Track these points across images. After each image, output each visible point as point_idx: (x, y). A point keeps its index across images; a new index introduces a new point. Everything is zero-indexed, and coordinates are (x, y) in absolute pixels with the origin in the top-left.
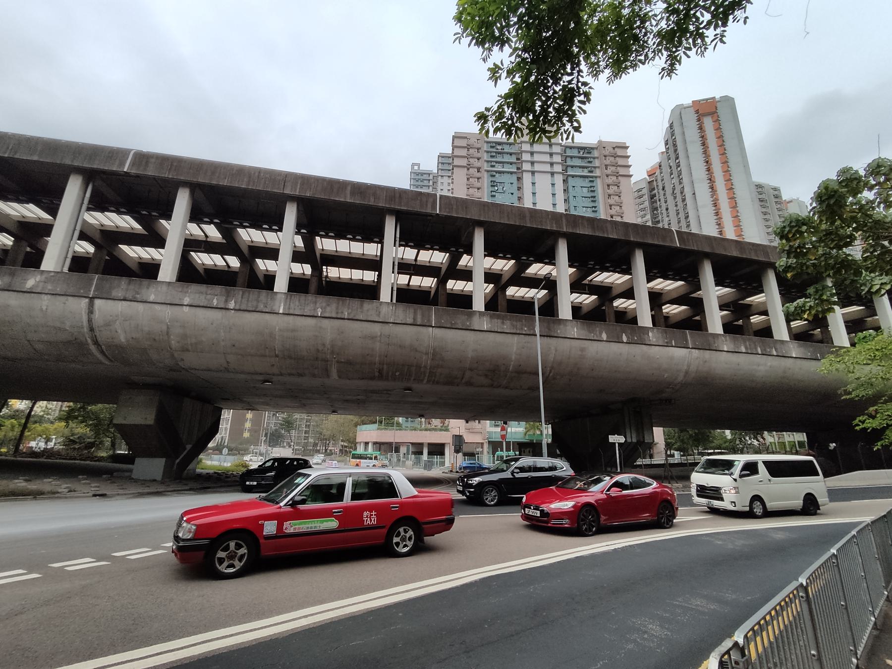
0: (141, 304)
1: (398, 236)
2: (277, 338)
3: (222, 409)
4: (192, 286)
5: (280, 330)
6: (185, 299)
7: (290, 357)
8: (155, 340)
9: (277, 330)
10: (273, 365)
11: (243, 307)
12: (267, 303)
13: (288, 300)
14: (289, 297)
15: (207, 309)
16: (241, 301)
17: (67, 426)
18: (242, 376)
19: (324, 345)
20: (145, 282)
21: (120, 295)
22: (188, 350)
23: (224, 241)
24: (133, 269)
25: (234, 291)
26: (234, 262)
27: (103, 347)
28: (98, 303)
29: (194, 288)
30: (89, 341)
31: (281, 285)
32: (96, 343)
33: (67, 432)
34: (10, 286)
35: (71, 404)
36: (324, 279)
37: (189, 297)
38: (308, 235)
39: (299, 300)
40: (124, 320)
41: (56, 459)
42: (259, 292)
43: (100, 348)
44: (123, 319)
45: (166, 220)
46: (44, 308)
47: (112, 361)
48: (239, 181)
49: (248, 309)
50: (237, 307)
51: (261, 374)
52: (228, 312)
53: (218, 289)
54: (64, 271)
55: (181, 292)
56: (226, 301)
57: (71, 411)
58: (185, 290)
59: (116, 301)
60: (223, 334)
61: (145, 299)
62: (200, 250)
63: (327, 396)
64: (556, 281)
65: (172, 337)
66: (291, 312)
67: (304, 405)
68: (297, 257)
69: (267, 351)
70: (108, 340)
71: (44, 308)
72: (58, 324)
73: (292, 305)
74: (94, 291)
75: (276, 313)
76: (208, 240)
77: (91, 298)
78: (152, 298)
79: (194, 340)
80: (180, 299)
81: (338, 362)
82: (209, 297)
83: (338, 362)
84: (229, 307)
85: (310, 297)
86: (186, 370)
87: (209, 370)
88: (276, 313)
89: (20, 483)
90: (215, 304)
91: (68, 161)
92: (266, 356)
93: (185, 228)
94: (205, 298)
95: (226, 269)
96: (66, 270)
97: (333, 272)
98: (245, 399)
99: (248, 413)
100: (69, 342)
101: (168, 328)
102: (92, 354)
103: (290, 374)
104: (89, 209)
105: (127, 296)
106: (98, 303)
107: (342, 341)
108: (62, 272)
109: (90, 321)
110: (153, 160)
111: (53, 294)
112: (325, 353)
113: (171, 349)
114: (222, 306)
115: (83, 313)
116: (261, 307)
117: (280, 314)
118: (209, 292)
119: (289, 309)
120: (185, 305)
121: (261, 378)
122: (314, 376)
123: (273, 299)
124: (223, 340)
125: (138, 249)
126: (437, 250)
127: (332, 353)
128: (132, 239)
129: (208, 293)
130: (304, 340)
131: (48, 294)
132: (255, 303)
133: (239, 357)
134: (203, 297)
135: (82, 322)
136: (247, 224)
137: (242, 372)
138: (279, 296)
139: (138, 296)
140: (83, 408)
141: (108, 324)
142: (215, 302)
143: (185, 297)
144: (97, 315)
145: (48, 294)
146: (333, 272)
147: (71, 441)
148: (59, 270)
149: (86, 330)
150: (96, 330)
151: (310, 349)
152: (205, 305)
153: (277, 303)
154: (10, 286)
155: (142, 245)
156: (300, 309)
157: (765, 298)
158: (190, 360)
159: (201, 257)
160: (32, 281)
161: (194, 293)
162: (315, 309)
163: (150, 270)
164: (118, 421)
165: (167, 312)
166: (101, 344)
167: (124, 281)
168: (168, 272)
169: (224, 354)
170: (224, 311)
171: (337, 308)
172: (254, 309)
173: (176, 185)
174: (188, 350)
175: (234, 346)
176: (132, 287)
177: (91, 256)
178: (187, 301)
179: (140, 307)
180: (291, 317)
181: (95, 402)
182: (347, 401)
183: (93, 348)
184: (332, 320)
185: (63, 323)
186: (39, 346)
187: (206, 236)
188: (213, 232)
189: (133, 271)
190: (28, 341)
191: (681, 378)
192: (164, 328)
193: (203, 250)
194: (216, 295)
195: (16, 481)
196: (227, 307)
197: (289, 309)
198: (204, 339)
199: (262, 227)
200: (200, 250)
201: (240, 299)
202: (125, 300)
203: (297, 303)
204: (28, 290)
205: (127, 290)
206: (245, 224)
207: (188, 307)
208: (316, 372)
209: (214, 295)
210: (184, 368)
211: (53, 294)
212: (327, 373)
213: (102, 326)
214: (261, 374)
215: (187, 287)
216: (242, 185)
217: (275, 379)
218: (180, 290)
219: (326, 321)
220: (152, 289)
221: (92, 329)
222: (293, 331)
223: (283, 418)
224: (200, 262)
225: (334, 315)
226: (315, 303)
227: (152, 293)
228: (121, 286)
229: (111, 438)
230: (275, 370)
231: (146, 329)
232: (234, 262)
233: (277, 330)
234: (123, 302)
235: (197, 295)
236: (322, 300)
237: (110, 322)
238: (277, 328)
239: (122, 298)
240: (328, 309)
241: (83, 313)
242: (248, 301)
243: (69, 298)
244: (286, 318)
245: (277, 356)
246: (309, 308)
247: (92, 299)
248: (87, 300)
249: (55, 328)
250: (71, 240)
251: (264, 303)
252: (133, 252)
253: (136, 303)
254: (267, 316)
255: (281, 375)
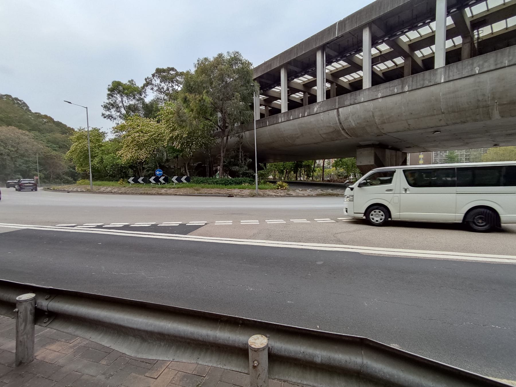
0: (358, 104)
1: (325, 59)
2: (442, 100)
3: (407, 153)
4: (381, 86)
5: (443, 95)
6: (379, 94)
7: (454, 112)
8: (368, 121)
9: (441, 95)
10: (441, 120)
11: (414, 87)
12: (431, 79)
13: (447, 71)
14: (447, 69)
15: (392, 96)
16: (412, 84)
17: (336, 169)
18: (419, 131)
19: (484, 95)
20: (358, 92)
21: (348, 103)
22: (385, 123)
23: (392, 50)
24: (347, 88)
25: (406, 79)
26: (400, 61)
27: (346, 130)
28: (340, 110)
29: (382, 86)
30: (340, 128)
31: (440, 62)
32: (343, 129)
33: (336, 172)
34: (310, 113)
35: (336, 159)
36: (476, 42)
37: (380, 92)
38: (458, 12)
39: (457, 67)
40: (352, 115)
41: (336, 182)
42: (424, 74)
43: (345, 131)
44: (352, 115)
45: (358, 54)
46: (322, 119)
47: (351, 136)
48: (397, 2)
49: (418, 88)
50: (410, 89)
51: (431, 128)
52: (404, 94)
53: (396, 82)
54: (325, 100)
55: (376, 91)
56: (403, 88)
57: (336, 162)
58: (378, 89)
59: (347, 107)
60: (403, 108)
61: (359, 101)
62: (378, 62)
63: (489, 134)
64: (330, 98)
65: (376, 118)
66: (451, 78)
67: (467, 143)
68: (450, 34)
69: (435, 111)
70: (348, 127)
71: (322, 119)
72: (328, 125)
73: (451, 74)
74: (338, 105)
75: (438, 84)
76: (382, 53)
77: (337, 109)
78: (362, 100)
79: (387, 117)
80: (376, 95)
81: (499, 105)
82: (391, 89)
83: (499, 105)
84: (405, 91)
85: (466, 62)
86: (385, 134)
87: (398, 132)
88: (438, 84)
89: (330, 191)
90: (396, 92)
91: (356, 26)
92: (434, 115)
93: (370, 51)
94: (390, 90)
95: (395, 67)
96: (325, 98)
97: (485, 32)
98: (421, 146)
99: (420, 155)
100: (332, 132)
101: (373, 113)
102: (343, 135)
103: (454, 124)
104: (326, 66)
105: (351, 103)
106: (340, 110)
107: (504, 87)
108: (324, 101)
109: (339, 119)
110: (347, 22)
111: (323, 112)
112: (486, 101)
113: (376, 124)
114: (400, 91)
115: (336, 117)
116: (427, 83)
117: (442, 83)
118: (391, 86)
119: (449, 77)
120: (379, 98)
121: (432, 130)
122: (476, 120)
123: (435, 75)
124: (404, 112)
125: (348, 77)
126: (430, 22)
127: (493, 99)
128: (344, 72)
129: (391, 86)
130: (464, 96)
131: (322, 112)
132: (422, 82)
133: (416, 119)
134: (388, 90)
135: (336, 121)
136: (429, 21)
137: (419, 129)
138: (439, 71)
139: (356, 101)
140: (340, 160)
141: (346, 119)
142: (396, 90)
143: (379, 93)
144: (341, 116)
145: (322, 112)
146: (485, 32)
147: (339, 175)
148: (323, 100)
149: (338, 124)
150: (342, 123)
151: (470, 102)
152: (390, 94)
153: (438, 76)
154: (310, 113)
155: (349, 74)
156: (459, 74)
157: (241, 221)
158: (387, 128)
159: (359, 74)
160: (316, 108)
161: (383, 89)
162: (472, 70)
163: (357, 86)
164: (359, 164)
165: (371, 105)
166: (345, 129)
167: (348, 95)
168: (367, 84)
169: (406, 120)
170: (402, 94)
171: (496, 61)
172: (421, 86)
173: (360, 30)
174: (385, 123)
175: (411, 114)
176: (352, 97)
177: (330, 89)
178: (380, 95)
179: (358, 106)
180: (452, 83)
181: (344, 158)
182: (510, 135)
183: (342, 132)
184: (491, 72)
185: (330, 124)
186: (324, 136)
187: (381, 52)
188: (384, 47)
189: (347, 89)
190: (320, 134)
191: (162, 344)
192: (371, 114)
193: (380, 61)
194: (396, 86)
195: (329, 190)
196: (403, 91)
197: (449, 77)
198: (393, 115)
199: (333, 61)
200: (378, 62)
201: (411, 83)
202: (351, 105)
203: (455, 70)
204: (316, 113)
205: (351, 99)
206: (427, 22)
207: (381, 99)
208: (478, 117)
209: (394, 86)
210: (384, 133)
211: (323, 112)
212: (488, 115)
213: (344, 121)
214: (431, 128)
215: (378, 87)
216: (400, 3)
217: (442, 129)
218: (375, 90)
219: (485, 75)
220: (361, 95)
221: (340, 123)
222: (454, 92)
223: (446, 155)
224: (379, 70)
225: (492, 68)
226: (472, 64)
227: (362, 96)
228: (348, 98)
229: (354, 173)
230: (443, 123)
231: (363, 117)
232: (400, 61)
233: (441, 95)
234: (350, 106)
235: (385, 90)
236: (478, 60)
237: (347, 118)
238: (441, 93)
239: (349, 104)
240: (486, 64)
241: (336, 117)
242: (417, 82)
243: (329, 111)
244: (447, 85)
245: (443, 113)
246: (466, 70)
247: (338, 109)
248: (336, 110)
249: (327, 126)
250: (324, 83)
251: (429, 80)
252: (346, 79)
253: (355, 105)
254: (432, 88)
255: (448, 125)
